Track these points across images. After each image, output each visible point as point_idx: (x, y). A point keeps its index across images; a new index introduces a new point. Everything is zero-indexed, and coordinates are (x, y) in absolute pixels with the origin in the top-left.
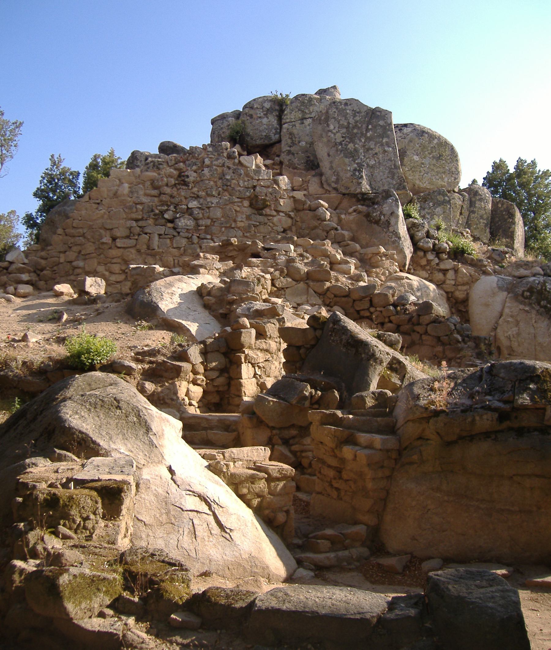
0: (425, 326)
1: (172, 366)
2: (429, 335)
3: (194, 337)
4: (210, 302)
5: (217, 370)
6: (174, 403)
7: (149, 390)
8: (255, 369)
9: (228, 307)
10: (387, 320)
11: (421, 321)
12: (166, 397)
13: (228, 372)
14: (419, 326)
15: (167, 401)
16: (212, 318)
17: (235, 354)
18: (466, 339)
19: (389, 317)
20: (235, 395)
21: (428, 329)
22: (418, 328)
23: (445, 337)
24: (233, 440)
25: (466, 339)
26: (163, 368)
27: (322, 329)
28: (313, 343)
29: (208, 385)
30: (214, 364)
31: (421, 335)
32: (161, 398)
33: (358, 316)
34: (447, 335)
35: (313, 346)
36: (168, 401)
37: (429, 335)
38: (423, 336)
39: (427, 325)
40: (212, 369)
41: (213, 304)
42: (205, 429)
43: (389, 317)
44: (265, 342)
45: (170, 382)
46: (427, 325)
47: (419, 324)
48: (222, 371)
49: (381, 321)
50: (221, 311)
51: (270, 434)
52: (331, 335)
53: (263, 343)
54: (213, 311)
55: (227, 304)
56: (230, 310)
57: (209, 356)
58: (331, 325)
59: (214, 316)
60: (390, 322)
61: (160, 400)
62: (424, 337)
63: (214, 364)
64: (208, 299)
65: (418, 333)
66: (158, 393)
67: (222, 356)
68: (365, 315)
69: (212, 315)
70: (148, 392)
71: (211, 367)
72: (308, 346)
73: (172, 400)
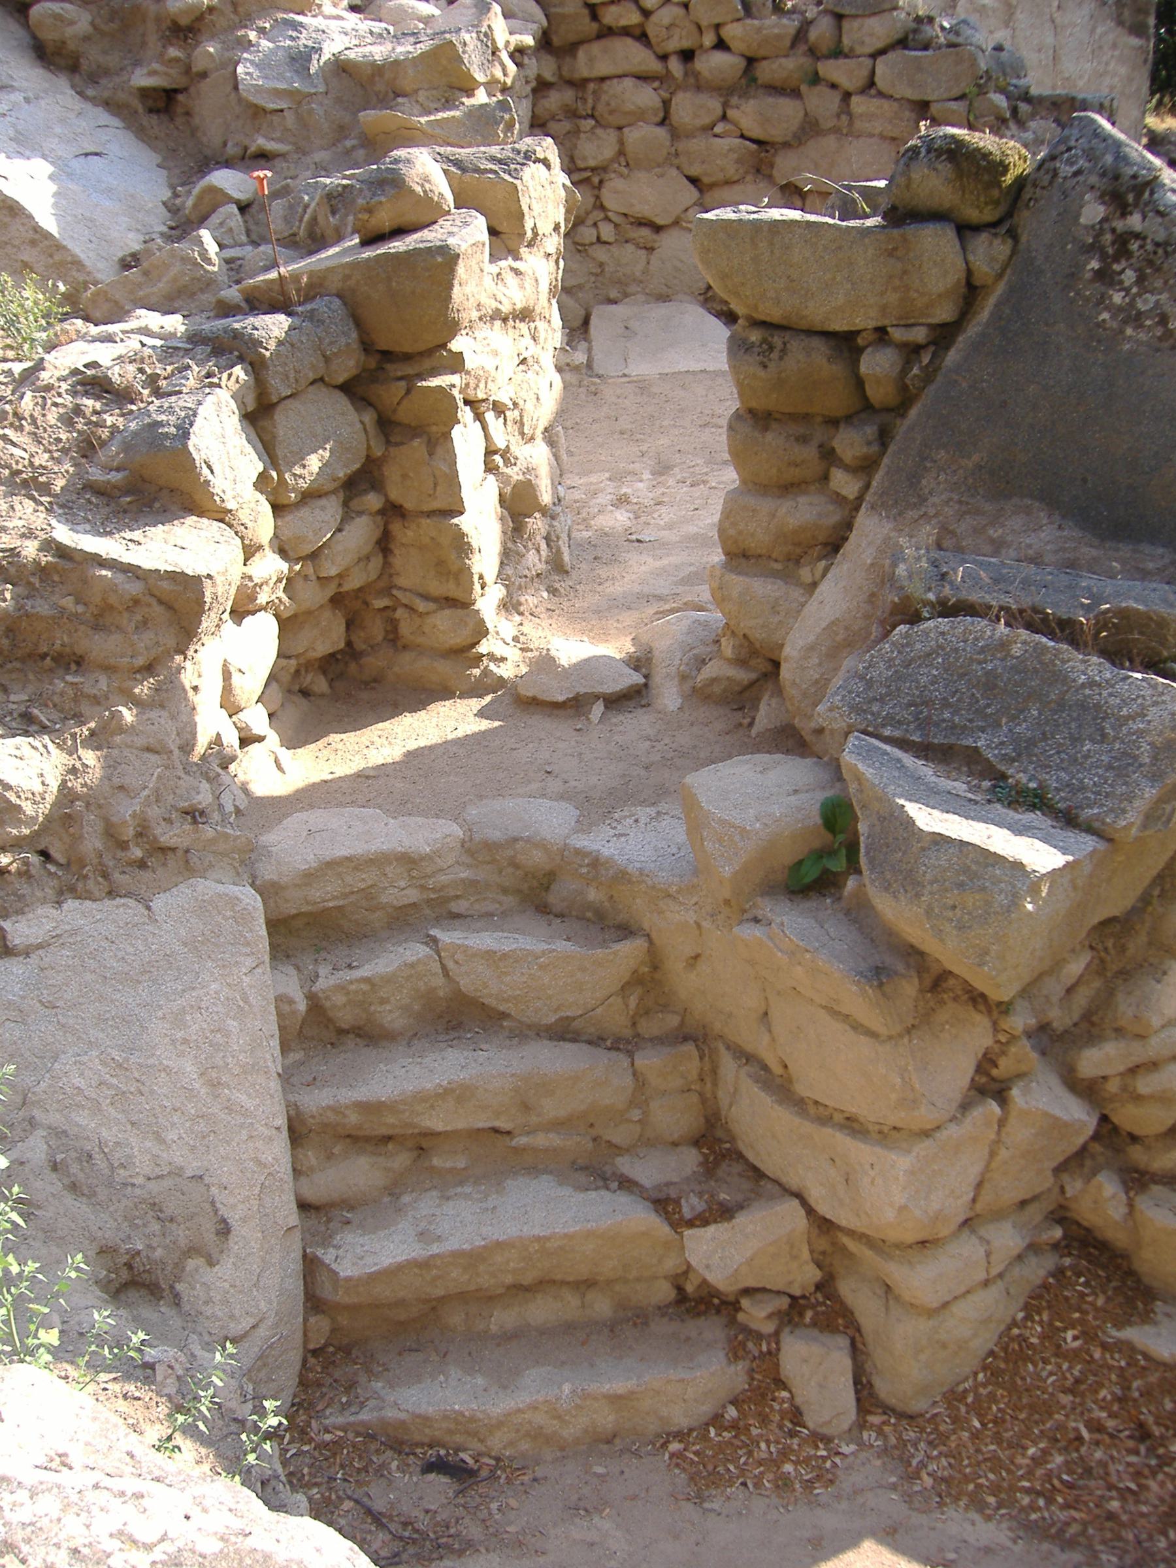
0: (868, 62)
1: (135, 588)
2: (881, 94)
3: (59, 247)
4: (69, 31)
5: (334, 492)
6: (208, 832)
7: (33, 798)
8: (484, 427)
9: (173, 52)
10: (709, 39)
11: (846, 41)
12: (154, 812)
13: (377, 485)
14: (841, 61)
15: (168, 836)
16: (104, 117)
17: (410, 379)
18: (1024, 107)
19: (718, 27)
20: (426, 597)
21: (878, 71)
22: (831, 70)
23: (953, 105)
24: (625, 989)
25: (1024, 107)
26: (68, 602)
27: (1004, 224)
28: (944, 313)
29: (299, 584)
30: (314, 463)
31: (847, 96)
32: (129, 833)
33: (595, 26)
34: (962, 97)
35: (944, 335)
36: (173, 835)
37: (881, 94)
38: (855, 100)
39: (874, 56)
40: (309, 496)
41: (87, 38)
42: (404, 921)
43: (718, 27)
44: (517, 272)
45: (143, 689)
46: (874, 56)
47: (838, 52)
48: (358, 482)
49: (686, 44)
50: (141, 79)
51: (988, 1041)
52: (1104, 276)
53: (509, 277)
54: (93, 79)
55: (167, 41)
56: (188, 70)
57: (284, 422)
58: (1093, 212)
59: (110, 105)
60: (721, 45)
61: (123, 846)
62: (859, 104)
63: (314, 463)
64: (58, 17)
65: (834, 86)
66: (92, 800)
67: (343, 401)
68: (623, 22)
69: (93, 100)
70: (28, 808)
71: (303, 485)
72: (919, 335)
73: (194, 815)
